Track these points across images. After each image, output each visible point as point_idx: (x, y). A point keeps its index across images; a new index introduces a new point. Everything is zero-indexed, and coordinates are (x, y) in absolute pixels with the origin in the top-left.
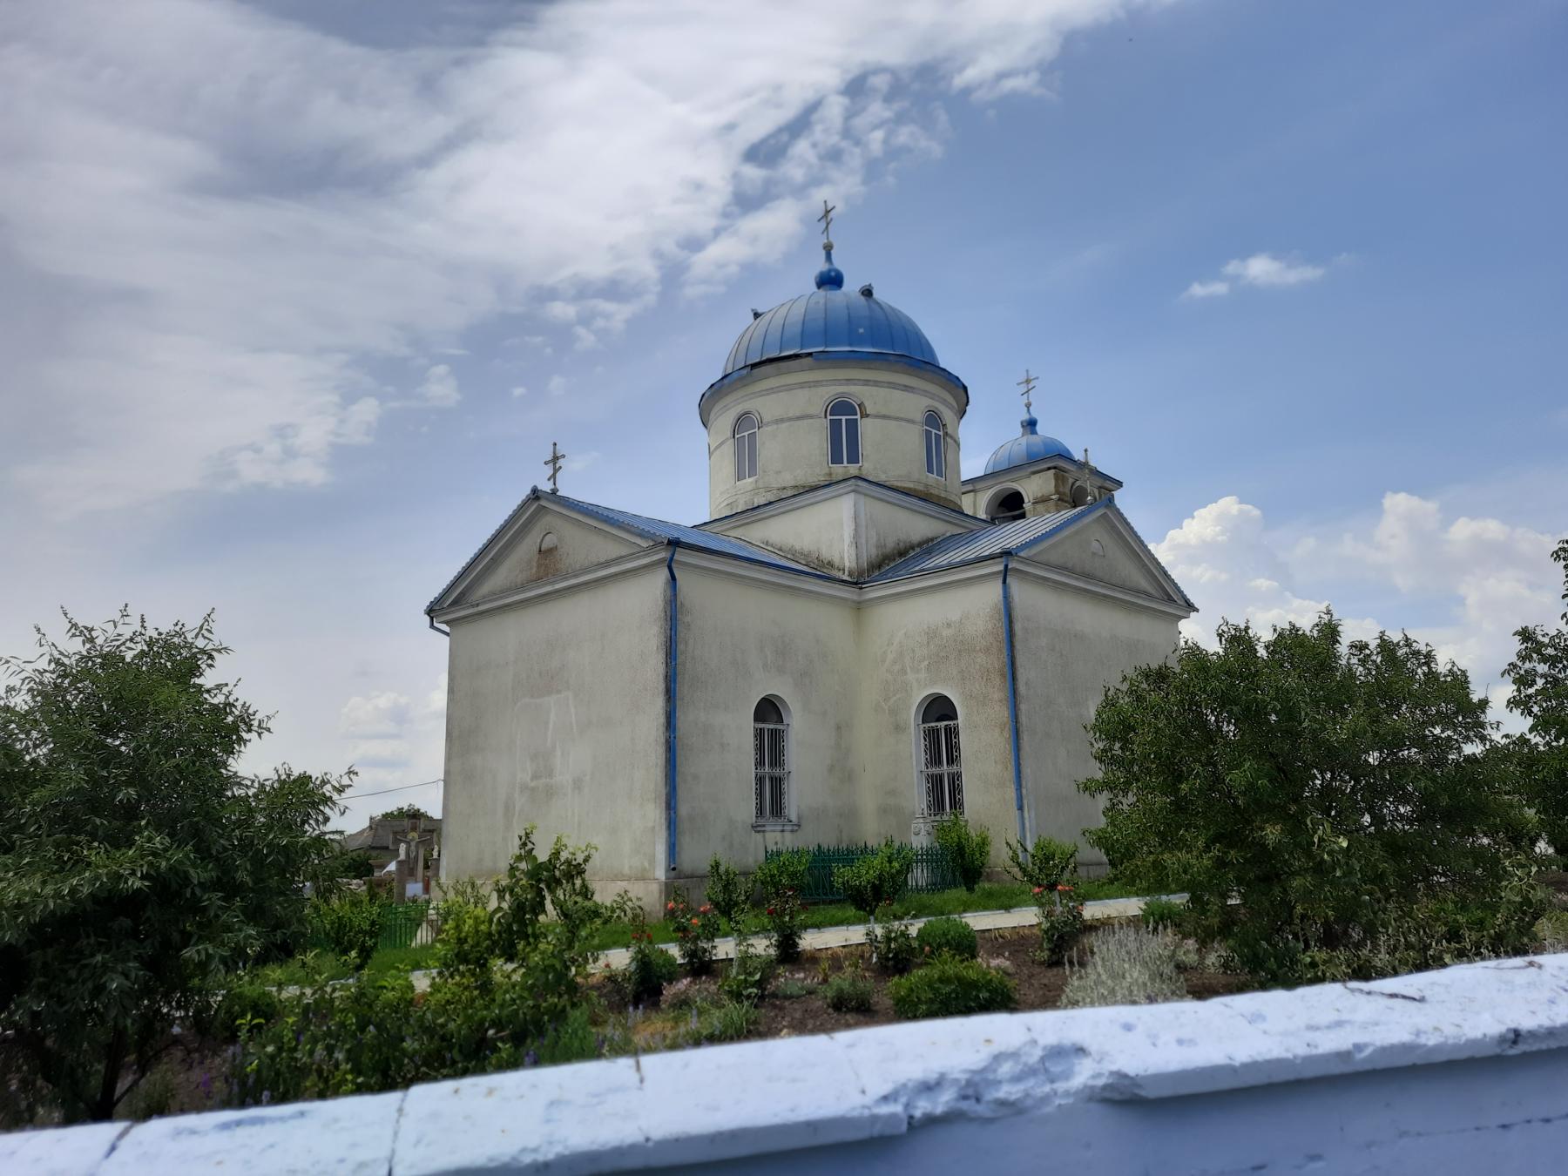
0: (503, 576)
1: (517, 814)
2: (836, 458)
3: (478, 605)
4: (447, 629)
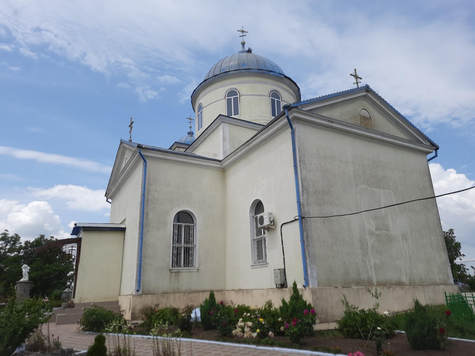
0: (335, 114)
1: (370, 248)
3: (333, 122)
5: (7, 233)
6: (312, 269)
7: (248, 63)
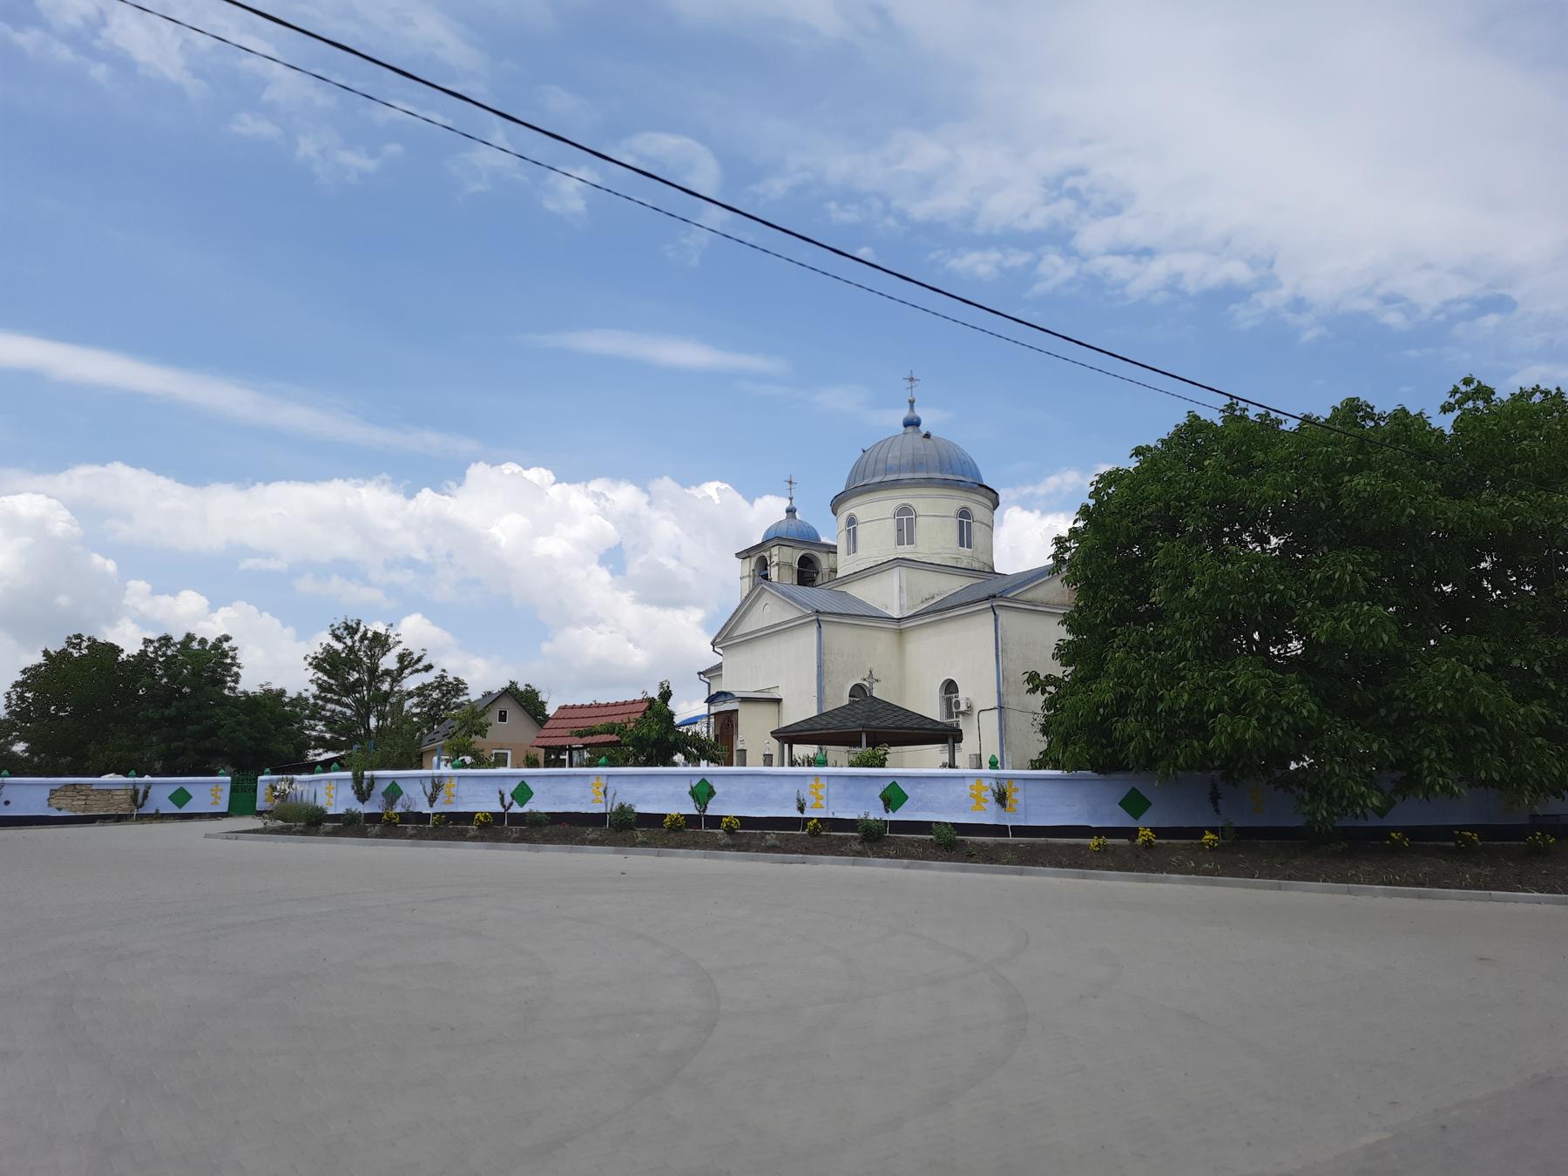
2: (900, 542)
4: (721, 652)
5: (445, 675)
6: (1007, 755)
7: (927, 462)
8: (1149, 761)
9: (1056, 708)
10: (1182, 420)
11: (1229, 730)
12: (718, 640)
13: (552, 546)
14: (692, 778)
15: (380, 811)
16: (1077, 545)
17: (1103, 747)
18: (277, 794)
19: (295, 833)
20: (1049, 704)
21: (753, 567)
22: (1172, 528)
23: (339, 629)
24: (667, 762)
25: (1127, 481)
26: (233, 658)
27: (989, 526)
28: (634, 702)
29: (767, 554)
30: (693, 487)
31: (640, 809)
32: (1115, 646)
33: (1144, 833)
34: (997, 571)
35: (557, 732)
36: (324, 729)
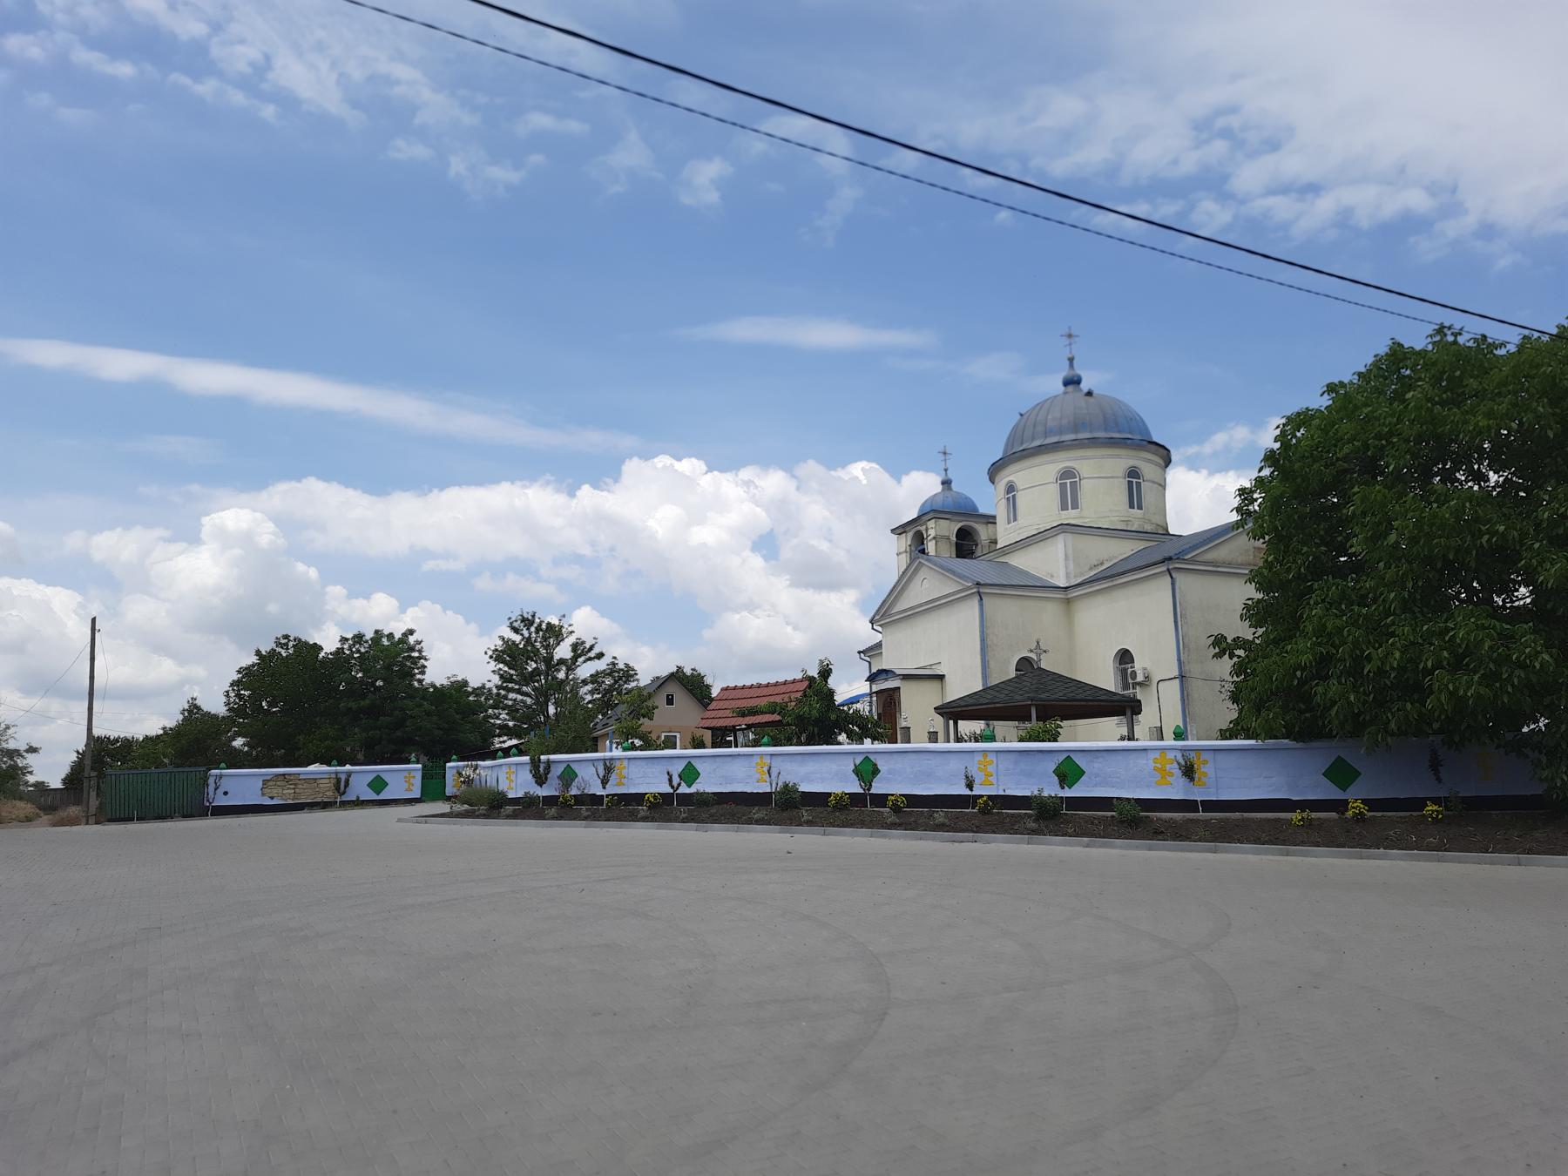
2: (1064, 507)
5: (616, 662)
8: (1355, 727)
9: (1246, 673)
10: (1383, 349)
11: (1451, 687)
12: (877, 618)
13: (706, 535)
14: (855, 756)
15: (557, 794)
16: (1263, 495)
17: (1301, 712)
18: (462, 779)
19: (478, 817)
20: (1239, 669)
21: (909, 543)
22: (1371, 469)
23: (516, 621)
24: (831, 740)
25: (1316, 422)
26: (420, 651)
27: (1160, 485)
28: (794, 681)
29: (923, 528)
30: (839, 469)
31: (804, 788)
32: (1312, 602)
33: (1355, 805)
34: (1171, 533)
35: (721, 713)
36: (507, 717)
